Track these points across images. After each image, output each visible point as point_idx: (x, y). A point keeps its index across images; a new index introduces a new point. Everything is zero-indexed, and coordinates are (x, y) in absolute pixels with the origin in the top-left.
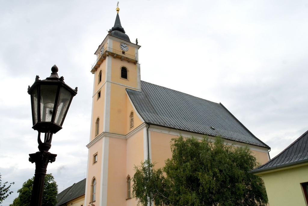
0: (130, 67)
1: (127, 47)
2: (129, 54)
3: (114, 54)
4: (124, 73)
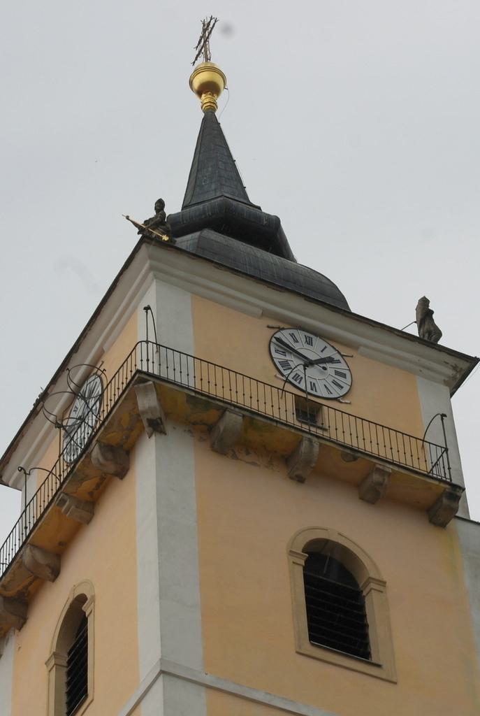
0: (383, 546)
1: (342, 367)
2: (367, 410)
3: (223, 407)
4: (336, 610)
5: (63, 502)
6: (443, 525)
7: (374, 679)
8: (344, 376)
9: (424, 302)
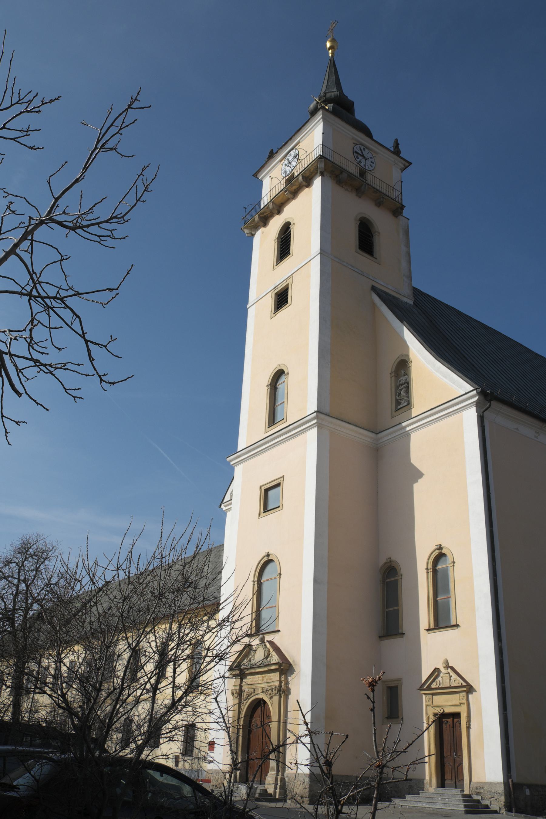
0: (381, 220)
4: (366, 240)
5: (286, 191)
6: (397, 217)
7: (272, 480)
8: (373, 163)
9: (396, 140)
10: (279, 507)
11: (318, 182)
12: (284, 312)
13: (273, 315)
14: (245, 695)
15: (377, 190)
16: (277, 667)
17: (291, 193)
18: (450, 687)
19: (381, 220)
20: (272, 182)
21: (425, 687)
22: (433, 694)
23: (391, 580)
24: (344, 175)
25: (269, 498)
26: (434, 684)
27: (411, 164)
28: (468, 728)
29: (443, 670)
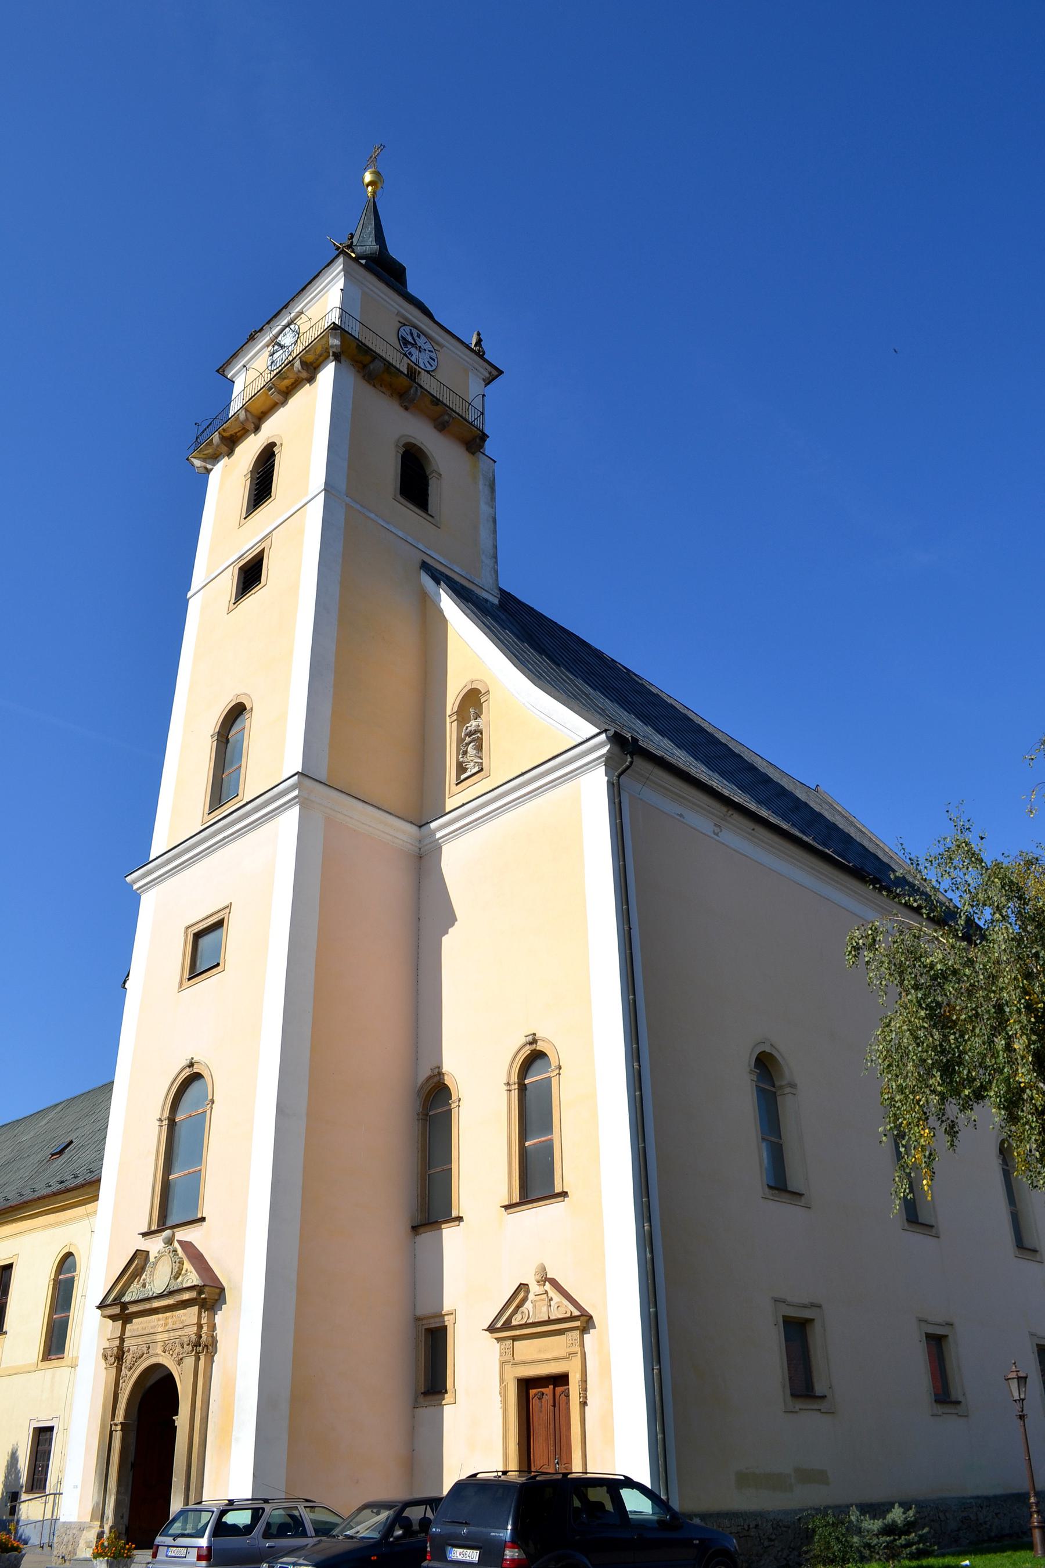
0: (443, 454)
3: (375, 356)
4: (415, 481)
5: (270, 389)
6: (473, 454)
7: (210, 913)
10: (218, 965)
11: (327, 374)
12: (256, 598)
13: (232, 606)
14: (129, 1357)
15: (439, 400)
16: (193, 1295)
17: (280, 392)
18: (549, 1322)
19: (443, 454)
20: (249, 377)
21: (499, 1325)
22: (514, 1339)
23: (439, 1111)
24: (377, 365)
25: (204, 948)
26: (518, 1316)
27: (501, 372)
28: (584, 1404)
29: (534, 1288)
